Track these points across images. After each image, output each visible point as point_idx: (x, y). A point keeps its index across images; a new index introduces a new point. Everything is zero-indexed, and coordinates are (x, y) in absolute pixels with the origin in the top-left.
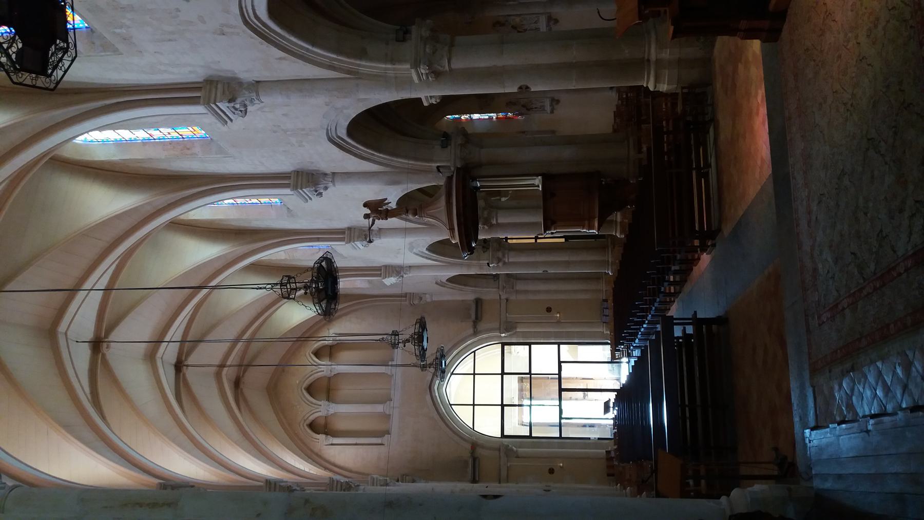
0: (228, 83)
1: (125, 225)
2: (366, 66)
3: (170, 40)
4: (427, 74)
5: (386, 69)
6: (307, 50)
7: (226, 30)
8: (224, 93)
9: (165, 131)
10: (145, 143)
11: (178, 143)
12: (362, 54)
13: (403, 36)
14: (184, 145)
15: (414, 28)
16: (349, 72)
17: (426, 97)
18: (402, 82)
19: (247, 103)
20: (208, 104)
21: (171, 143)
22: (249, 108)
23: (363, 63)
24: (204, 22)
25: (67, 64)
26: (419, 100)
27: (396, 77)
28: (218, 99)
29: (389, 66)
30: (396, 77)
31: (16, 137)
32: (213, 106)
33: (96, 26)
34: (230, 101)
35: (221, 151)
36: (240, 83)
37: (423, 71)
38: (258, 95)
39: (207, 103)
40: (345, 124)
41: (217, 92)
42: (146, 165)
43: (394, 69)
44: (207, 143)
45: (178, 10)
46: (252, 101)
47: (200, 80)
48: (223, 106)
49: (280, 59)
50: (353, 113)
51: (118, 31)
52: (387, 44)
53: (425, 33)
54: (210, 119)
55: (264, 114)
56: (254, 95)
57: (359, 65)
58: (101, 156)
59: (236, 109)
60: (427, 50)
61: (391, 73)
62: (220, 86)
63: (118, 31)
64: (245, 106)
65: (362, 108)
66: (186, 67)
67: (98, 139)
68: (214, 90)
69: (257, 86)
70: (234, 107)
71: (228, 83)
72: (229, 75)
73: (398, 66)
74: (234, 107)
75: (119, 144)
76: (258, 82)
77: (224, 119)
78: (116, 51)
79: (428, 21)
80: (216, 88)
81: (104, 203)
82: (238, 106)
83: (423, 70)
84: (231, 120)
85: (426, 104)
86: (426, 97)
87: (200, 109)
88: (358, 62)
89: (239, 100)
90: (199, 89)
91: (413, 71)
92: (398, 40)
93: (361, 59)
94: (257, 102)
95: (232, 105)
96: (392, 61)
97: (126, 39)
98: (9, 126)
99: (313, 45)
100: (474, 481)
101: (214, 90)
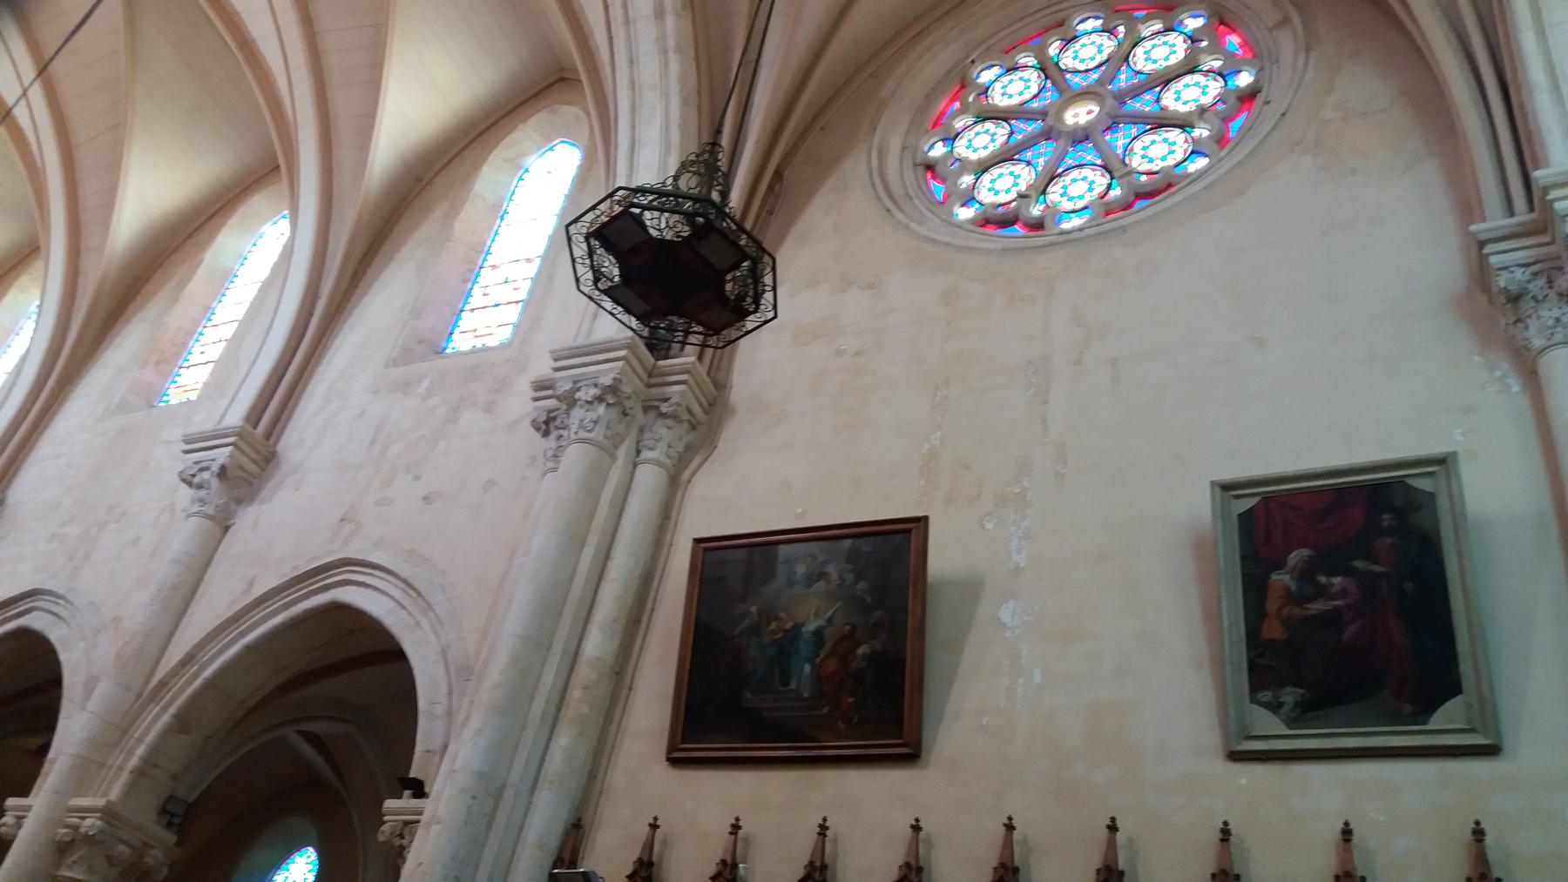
0: (250, 484)
1: (90, 187)
2: (157, 722)
3: (373, 442)
4: (76, 828)
5: (130, 754)
6: (243, 634)
7: (348, 528)
8: (241, 468)
9: (215, 352)
10: (207, 311)
11: (178, 355)
12: (182, 723)
13: (176, 814)
14: (168, 359)
15: (170, 837)
16: (163, 685)
17: (28, 809)
18: (86, 771)
19: (202, 493)
20: (239, 435)
21: (185, 345)
22: (186, 493)
23: (166, 718)
24: (377, 503)
25: (581, 270)
26: (24, 791)
27: (102, 765)
28: (237, 453)
29: (134, 761)
30: (102, 765)
31: (344, 156)
32: (231, 440)
33: (439, 362)
34: (223, 468)
35: (123, 407)
36: (239, 501)
37: (88, 822)
38: (208, 517)
39: (240, 434)
40: (55, 634)
41: (246, 461)
42: (171, 284)
43: (121, 769)
44: (150, 396)
45: (417, 478)
46: (202, 501)
47: (280, 447)
48: (222, 455)
49: (251, 584)
50: (72, 661)
51: (426, 383)
52: (174, 777)
53: (155, 856)
54: (203, 422)
55: (161, 511)
56: (210, 510)
57: (165, 709)
58: (225, 242)
59: (201, 470)
60: (122, 847)
61: (116, 759)
62: (253, 468)
63: (426, 383)
64: (199, 487)
65: (67, 681)
66: (311, 436)
67: (261, 254)
68: (255, 457)
69: (224, 525)
70: (207, 469)
71: (250, 484)
72: (265, 493)
73: (124, 777)
74: (207, 469)
75: (225, 278)
76: (227, 529)
77: (194, 443)
78: (394, 362)
79: (165, 871)
80: (254, 462)
81: (149, 189)
82: (206, 475)
83: (91, 824)
84: (536, 399)
85: (11, 802)
86: (28, 809)
87: (235, 417)
88: (173, 710)
89: (215, 483)
90: (268, 436)
91: (100, 802)
92: (171, 798)
93: (176, 716)
94: (196, 508)
95: (215, 467)
96: (140, 773)
97: (406, 386)
98: (364, 166)
99: (248, 649)
100: (277, 167)
101: (255, 457)
